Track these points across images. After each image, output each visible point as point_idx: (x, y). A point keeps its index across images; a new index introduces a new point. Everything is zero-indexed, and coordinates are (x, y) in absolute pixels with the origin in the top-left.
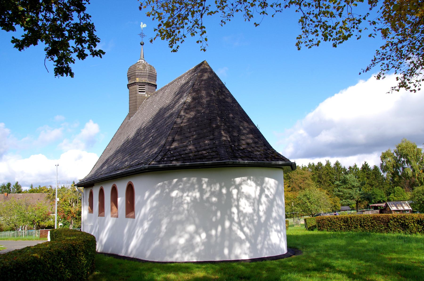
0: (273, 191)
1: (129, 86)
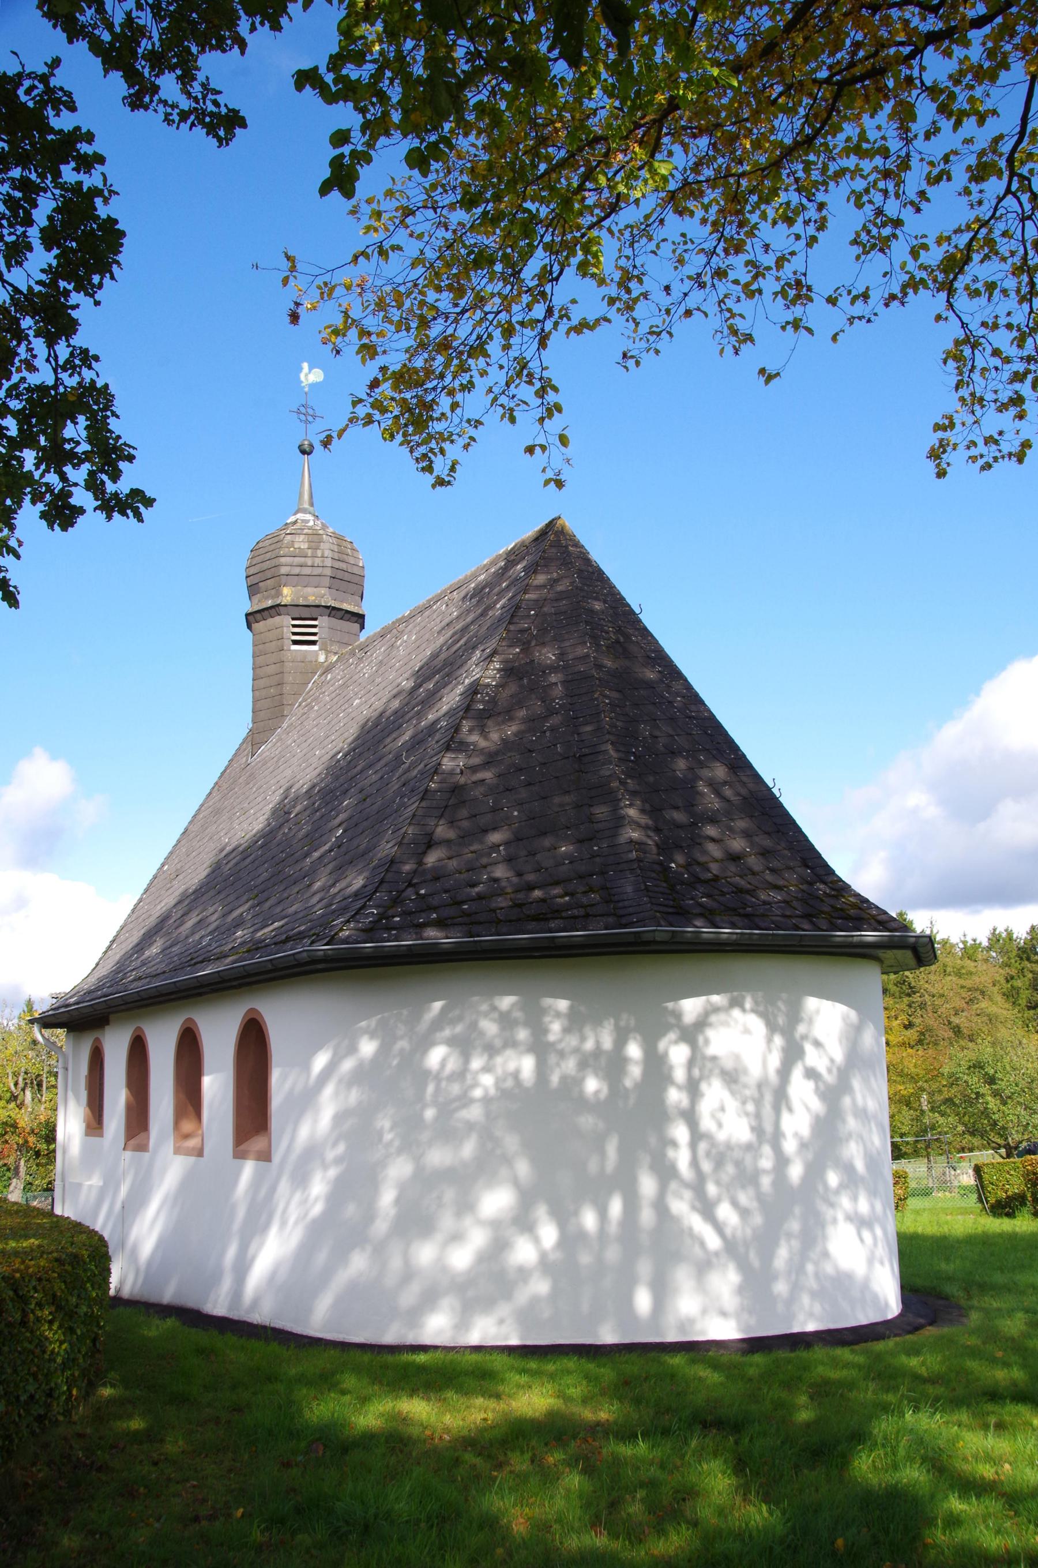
0: (838, 1053)
1: (252, 618)
